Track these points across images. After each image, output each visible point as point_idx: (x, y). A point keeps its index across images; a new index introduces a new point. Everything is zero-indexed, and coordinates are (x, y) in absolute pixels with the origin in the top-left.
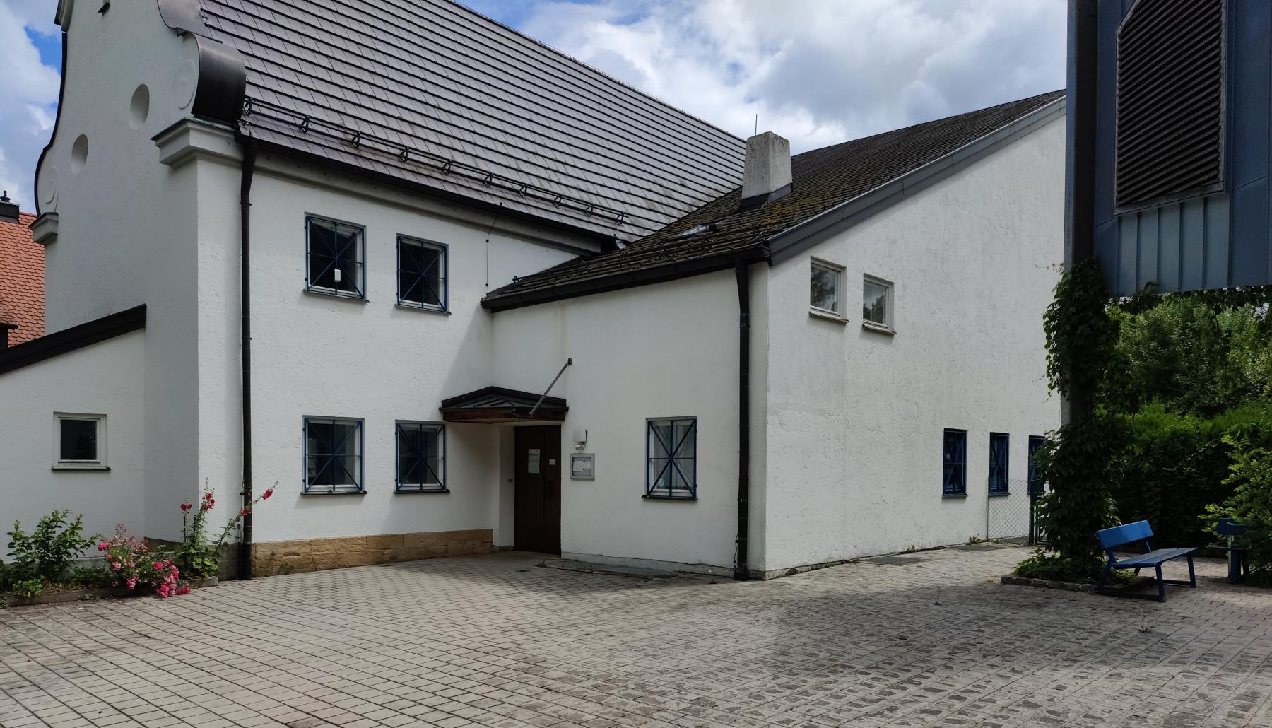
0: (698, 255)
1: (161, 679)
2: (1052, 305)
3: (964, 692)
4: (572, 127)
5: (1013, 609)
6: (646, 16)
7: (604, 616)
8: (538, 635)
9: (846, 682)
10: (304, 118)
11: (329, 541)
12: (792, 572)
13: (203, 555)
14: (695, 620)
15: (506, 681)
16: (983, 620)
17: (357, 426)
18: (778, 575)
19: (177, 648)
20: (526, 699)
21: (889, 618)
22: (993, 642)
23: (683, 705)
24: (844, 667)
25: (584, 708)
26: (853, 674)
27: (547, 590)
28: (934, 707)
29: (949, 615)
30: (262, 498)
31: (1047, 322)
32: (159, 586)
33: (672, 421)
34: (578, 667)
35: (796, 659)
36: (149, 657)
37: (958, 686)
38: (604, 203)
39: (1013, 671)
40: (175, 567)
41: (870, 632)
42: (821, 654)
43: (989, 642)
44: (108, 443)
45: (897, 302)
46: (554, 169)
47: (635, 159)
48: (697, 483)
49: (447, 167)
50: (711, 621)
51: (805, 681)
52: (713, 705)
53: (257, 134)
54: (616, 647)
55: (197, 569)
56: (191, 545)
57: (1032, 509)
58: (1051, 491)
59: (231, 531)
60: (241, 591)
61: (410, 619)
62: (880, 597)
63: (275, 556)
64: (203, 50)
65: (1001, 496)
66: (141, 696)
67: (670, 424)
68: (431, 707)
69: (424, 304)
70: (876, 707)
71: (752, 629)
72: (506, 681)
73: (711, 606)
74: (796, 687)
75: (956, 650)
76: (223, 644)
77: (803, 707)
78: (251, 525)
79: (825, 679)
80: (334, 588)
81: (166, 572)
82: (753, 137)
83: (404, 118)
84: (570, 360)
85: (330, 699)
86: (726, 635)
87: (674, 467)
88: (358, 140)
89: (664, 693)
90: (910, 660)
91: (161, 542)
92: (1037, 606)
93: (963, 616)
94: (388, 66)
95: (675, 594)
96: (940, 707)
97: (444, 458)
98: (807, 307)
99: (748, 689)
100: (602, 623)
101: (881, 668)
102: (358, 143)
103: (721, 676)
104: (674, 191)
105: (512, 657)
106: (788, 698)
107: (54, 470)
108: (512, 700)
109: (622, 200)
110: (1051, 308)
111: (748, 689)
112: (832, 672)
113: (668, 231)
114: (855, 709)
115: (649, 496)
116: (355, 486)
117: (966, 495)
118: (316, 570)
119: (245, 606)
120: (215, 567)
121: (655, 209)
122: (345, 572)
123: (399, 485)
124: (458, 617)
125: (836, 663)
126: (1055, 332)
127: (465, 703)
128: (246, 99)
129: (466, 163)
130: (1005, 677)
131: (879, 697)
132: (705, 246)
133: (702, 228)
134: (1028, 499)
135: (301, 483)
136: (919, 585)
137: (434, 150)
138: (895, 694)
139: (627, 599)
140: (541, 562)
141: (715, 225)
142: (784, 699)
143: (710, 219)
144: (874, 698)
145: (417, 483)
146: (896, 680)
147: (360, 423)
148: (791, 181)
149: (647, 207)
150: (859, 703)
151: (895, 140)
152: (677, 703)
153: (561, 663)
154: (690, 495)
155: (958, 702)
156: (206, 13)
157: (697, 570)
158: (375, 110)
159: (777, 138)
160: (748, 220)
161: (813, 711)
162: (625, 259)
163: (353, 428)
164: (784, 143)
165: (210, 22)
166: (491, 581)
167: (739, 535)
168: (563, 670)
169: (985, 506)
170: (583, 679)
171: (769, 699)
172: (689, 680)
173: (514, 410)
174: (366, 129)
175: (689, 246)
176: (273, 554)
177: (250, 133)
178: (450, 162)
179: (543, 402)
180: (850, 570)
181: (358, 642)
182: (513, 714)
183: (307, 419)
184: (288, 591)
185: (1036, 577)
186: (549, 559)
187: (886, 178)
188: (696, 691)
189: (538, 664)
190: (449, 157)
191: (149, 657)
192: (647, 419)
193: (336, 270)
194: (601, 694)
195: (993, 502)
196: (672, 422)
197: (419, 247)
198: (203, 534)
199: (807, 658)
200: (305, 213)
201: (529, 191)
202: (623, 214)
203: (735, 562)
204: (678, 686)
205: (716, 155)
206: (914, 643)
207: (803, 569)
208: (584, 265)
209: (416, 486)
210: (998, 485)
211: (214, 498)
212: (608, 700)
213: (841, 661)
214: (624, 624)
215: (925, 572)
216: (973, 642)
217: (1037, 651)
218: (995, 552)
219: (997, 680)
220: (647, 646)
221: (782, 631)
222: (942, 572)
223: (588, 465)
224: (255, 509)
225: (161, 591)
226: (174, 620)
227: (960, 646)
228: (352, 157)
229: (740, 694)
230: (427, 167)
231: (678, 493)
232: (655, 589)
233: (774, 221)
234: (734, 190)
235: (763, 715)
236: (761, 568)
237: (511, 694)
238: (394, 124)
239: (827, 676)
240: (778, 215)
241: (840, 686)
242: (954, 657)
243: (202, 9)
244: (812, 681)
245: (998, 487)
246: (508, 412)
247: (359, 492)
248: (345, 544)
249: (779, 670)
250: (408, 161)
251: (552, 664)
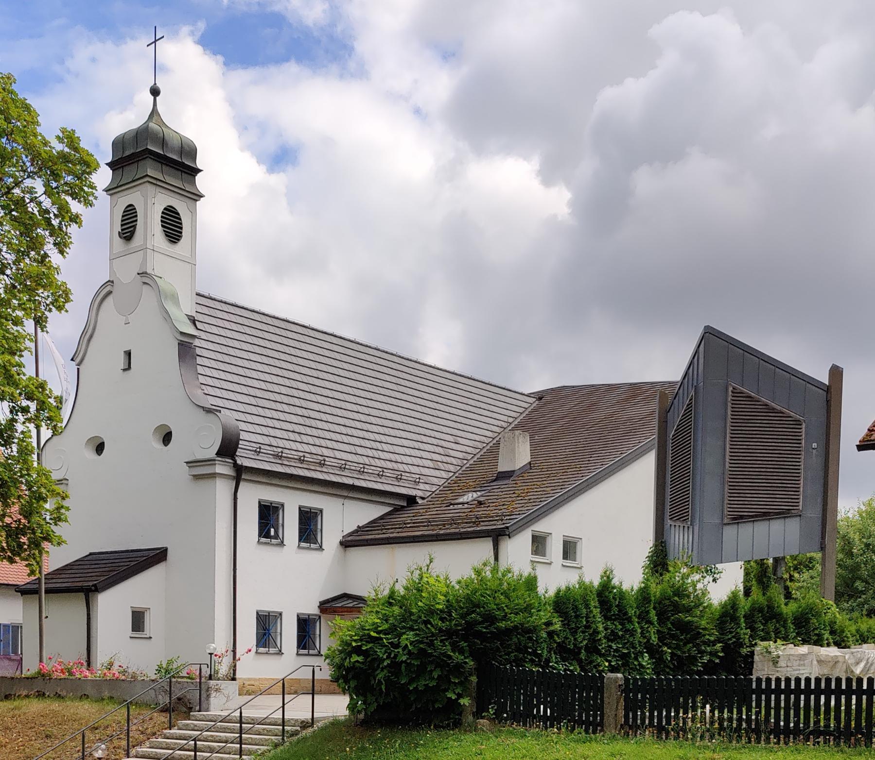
44: (151, 624)
97: (320, 635)
107: (131, 637)
176: (244, 684)
209: (305, 652)
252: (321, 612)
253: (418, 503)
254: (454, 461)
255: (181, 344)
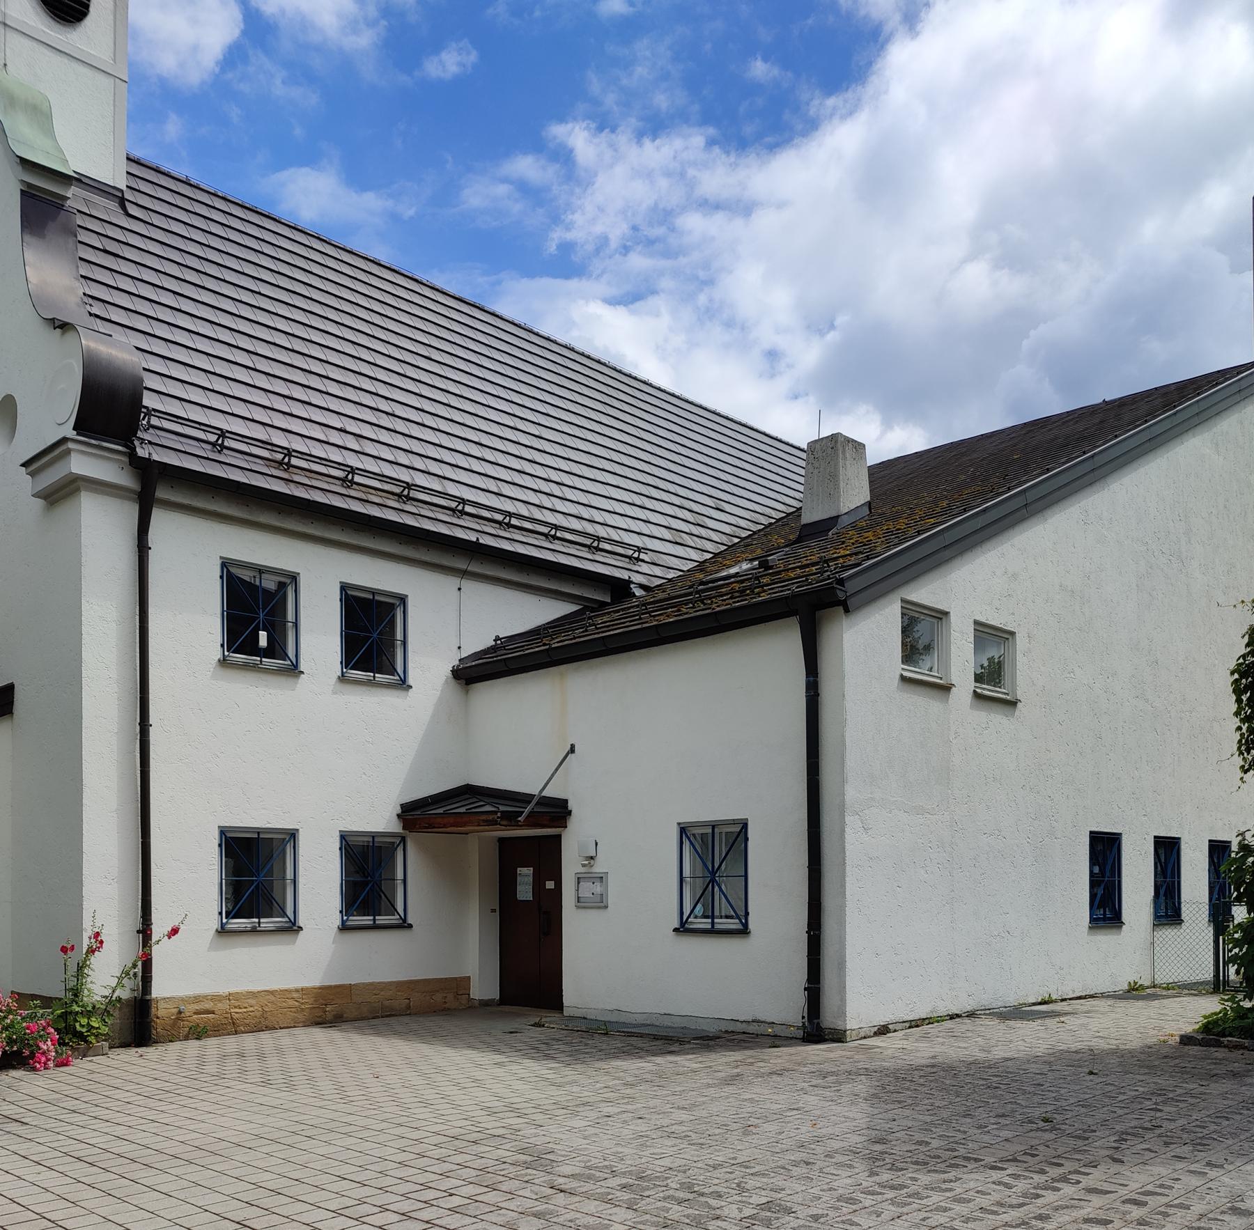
0: (746, 600)
1: (41, 1177)
2: (1244, 656)
3: (1144, 1194)
4: (526, 446)
5: (1201, 1079)
6: (654, 292)
7: (628, 1091)
8: (539, 1118)
9: (971, 1180)
10: (219, 432)
11: (253, 995)
12: (883, 1030)
13: (89, 1014)
14: (754, 1096)
15: (502, 1179)
16: (1160, 1095)
17: (289, 840)
18: (862, 1034)
19: (61, 1137)
20: (530, 1203)
21: (1024, 1092)
22: (1177, 1125)
23: (748, 1212)
24: (968, 1159)
25: (610, 1215)
26: (982, 1169)
27: (548, 1057)
28: (1102, 1215)
29: (1111, 1088)
30: (166, 937)
31: (1236, 680)
32: (32, 1055)
33: (714, 826)
34: (598, 1161)
35: (899, 1149)
36: (23, 1148)
37: (1134, 1186)
38: (614, 535)
39: (1209, 1164)
40: (52, 1030)
41: (1001, 1111)
42: (933, 1141)
43: (1172, 1126)
45: (1019, 656)
46: (546, 491)
47: (702, 453)
48: (750, 910)
49: (406, 492)
50: (775, 1097)
51: (915, 1179)
52: (789, 1211)
53: (158, 456)
54: (648, 1133)
55: (82, 1033)
56: (73, 1001)
57: (1216, 942)
58: (1250, 915)
59: (125, 981)
60: (141, 1061)
61: (365, 1097)
62: (1009, 1063)
63: (183, 1015)
64: (88, 347)
65: (1172, 924)
66: (15, 1200)
67: (710, 831)
68: (403, 1214)
69: (377, 675)
70: (1018, 1215)
71: (833, 1107)
72: (502, 1179)
73: (775, 1077)
74: (902, 1187)
75: (1124, 1136)
76: (120, 1131)
77: (915, 1214)
78: (151, 972)
79: (942, 1176)
80: (261, 1056)
81: (41, 1036)
82: (816, 441)
83: (348, 429)
84: (573, 747)
85: (266, 1203)
86: (799, 1116)
87: (716, 888)
88: (289, 459)
89: (719, 1196)
90: (1061, 1150)
91: (34, 997)
92: (1235, 1075)
93: (1130, 1090)
94: (327, 362)
95: (724, 1061)
96: (1111, 1215)
97: (405, 881)
98: (895, 665)
99: (835, 1190)
100: (626, 1100)
101: (1020, 1161)
102: (289, 464)
103: (796, 1171)
104: (708, 517)
105: (507, 1146)
106: (893, 1202)
108: (512, 1205)
109: (638, 531)
110: (1241, 661)
111: (835, 1190)
112: (951, 1166)
113: (701, 570)
114: (990, 1216)
115: (683, 929)
116: (287, 919)
117: (1122, 922)
118: (236, 1033)
119: (146, 1081)
120: (105, 1030)
121: (682, 542)
122: (275, 1035)
123: (345, 918)
124: (429, 1094)
125: (956, 1154)
126: (1248, 694)
127: (449, 1209)
128: (143, 410)
129: (430, 487)
130: (1200, 1173)
131: (1021, 1200)
132: (755, 588)
133: (745, 566)
134: (1211, 929)
135: (216, 916)
136: (1063, 1047)
137: (389, 471)
138: (1043, 1196)
139: (658, 1068)
140: (537, 1020)
141: (767, 560)
142: (886, 1203)
143: (759, 552)
144: (1014, 1202)
145: (368, 915)
146: (1044, 1178)
147: (293, 835)
148: (868, 499)
149: (672, 539)
150: (995, 1209)
151: (1009, 441)
152: (738, 1208)
153: (575, 1155)
154: (740, 927)
155: (1136, 1207)
156: (90, 299)
157: (753, 1028)
158: (310, 421)
159: (849, 441)
160: (812, 552)
161: (930, 1220)
162: (646, 609)
163: (283, 842)
164: (859, 447)
165: (95, 310)
166: (471, 1047)
167: (809, 980)
168: (578, 1164)
169: (1150, 939)
170: (606, 1176)
171: (867, 1203)
172: (752, 1177)
173: (499, 814)
174: (298, 445)
175: (732, 589)
176: (180, 1012)
177: (149, 454)
178: (409, 486)
179: (538, 804)
180: (964, 1028)
181: (298, 1128)
182: (515, 1224)
183: (223, 832)
184: (201, 1061)
185: (1231, 1035)
186: (546, 1017)
187: (1001, 490)
188: (763, 1193)
189: (543, 1156)
190: (408, 479)
191: (23, 1148)
192: (679, 824)
193: (260, 632)
194: (632, 1196)
195: (1160, 933)
196: (713, 827)
197: (369, 599)
198: (89, 986)
199: (914, 1147)
200: (221, 558)
201: (514, 521)
202: (639, 550)
203: (803, 1017)
204: (738, 1185)
205: (762, 468)
206: (1063, 1127)
207: (899, 1026)
208: (590, 618)
209: (367, 920)
210: (1167, 909)
211: (103, 937)
212: (642, 1204)
213: (962, 1151)
214: (657, 1102)
215: (1071, 1030)
216: (1148, 1125)
217: (1242, 1137)
218: (1165, 1001)
219: (1190, 1178)
220: (691, 1131)
221: (876, 1111)
222: (1095, 1029)
223: (598, 888)
224: (157, 952)
225: (36, 1062)
226: (54, 1099)
227: (1130, 1130)
228: (282, 482)
229: (826, 1196)
230: (380, 493)
231: (722, 923)
232: (694, 1056)
233: (848, 552)
234: (789, 515)
235: (861, 1225)
236: (839, 1025)
237: (510, 1196)
238: (335, 438)
239: (946, 1172)
240: (853, 544)
241: (964, 1186)
242: (1123, 1146)
243: (84, 294)
244: (925, 1179)
245: (1166, 912)
246: (491, 817)
247: (292, 928)
248: (274, 998)
249: (876, 1164)
250: (354, 486)
251: (563, 1156)
252: (404, 828)
253: (634, 595)
254: (714, 536)
255: (29, 196)
